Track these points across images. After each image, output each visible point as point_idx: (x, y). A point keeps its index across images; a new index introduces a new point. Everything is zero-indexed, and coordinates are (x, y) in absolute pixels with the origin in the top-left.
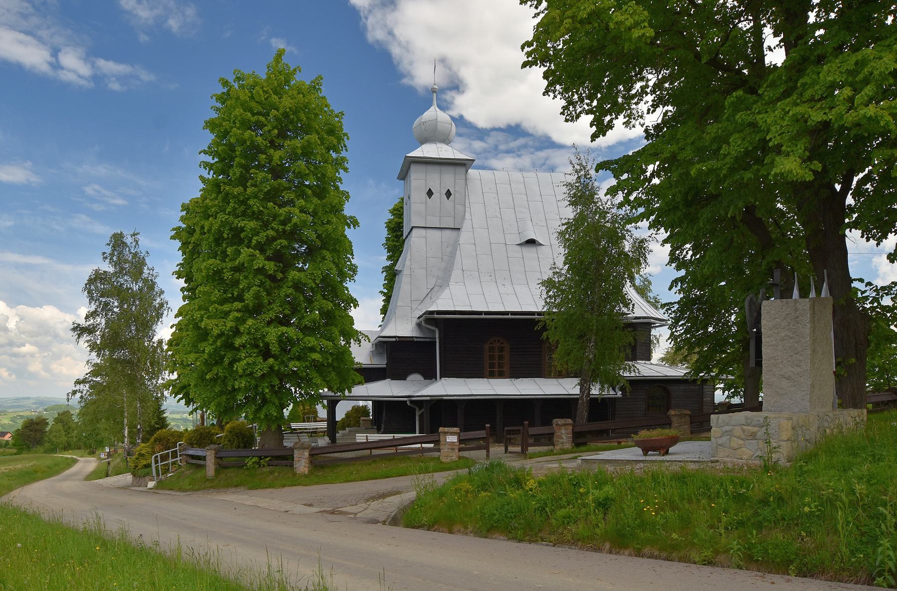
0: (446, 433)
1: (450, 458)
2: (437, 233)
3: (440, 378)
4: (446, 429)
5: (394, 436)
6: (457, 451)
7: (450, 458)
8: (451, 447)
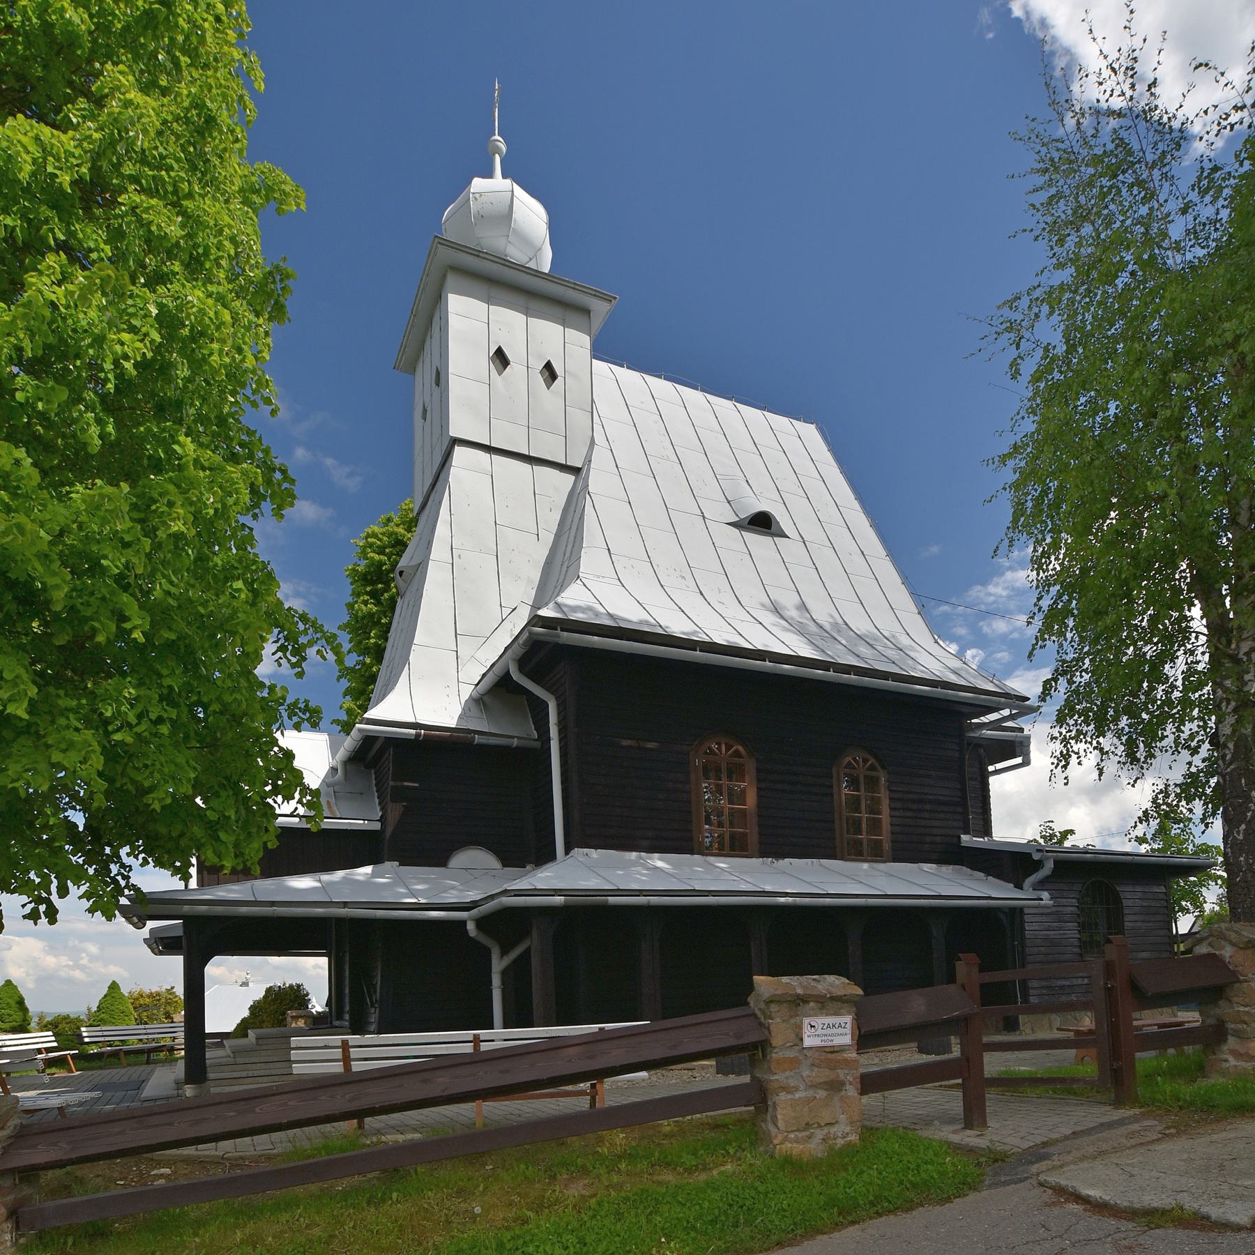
0: (798, 1002)
1: (820, 1134)
2: (525, 468)
3: (567, 851)
4: (795, 984)
5: (477, 1041)
6: (851, 1091)
7: (820, 1134)
8: (824, 1074)
